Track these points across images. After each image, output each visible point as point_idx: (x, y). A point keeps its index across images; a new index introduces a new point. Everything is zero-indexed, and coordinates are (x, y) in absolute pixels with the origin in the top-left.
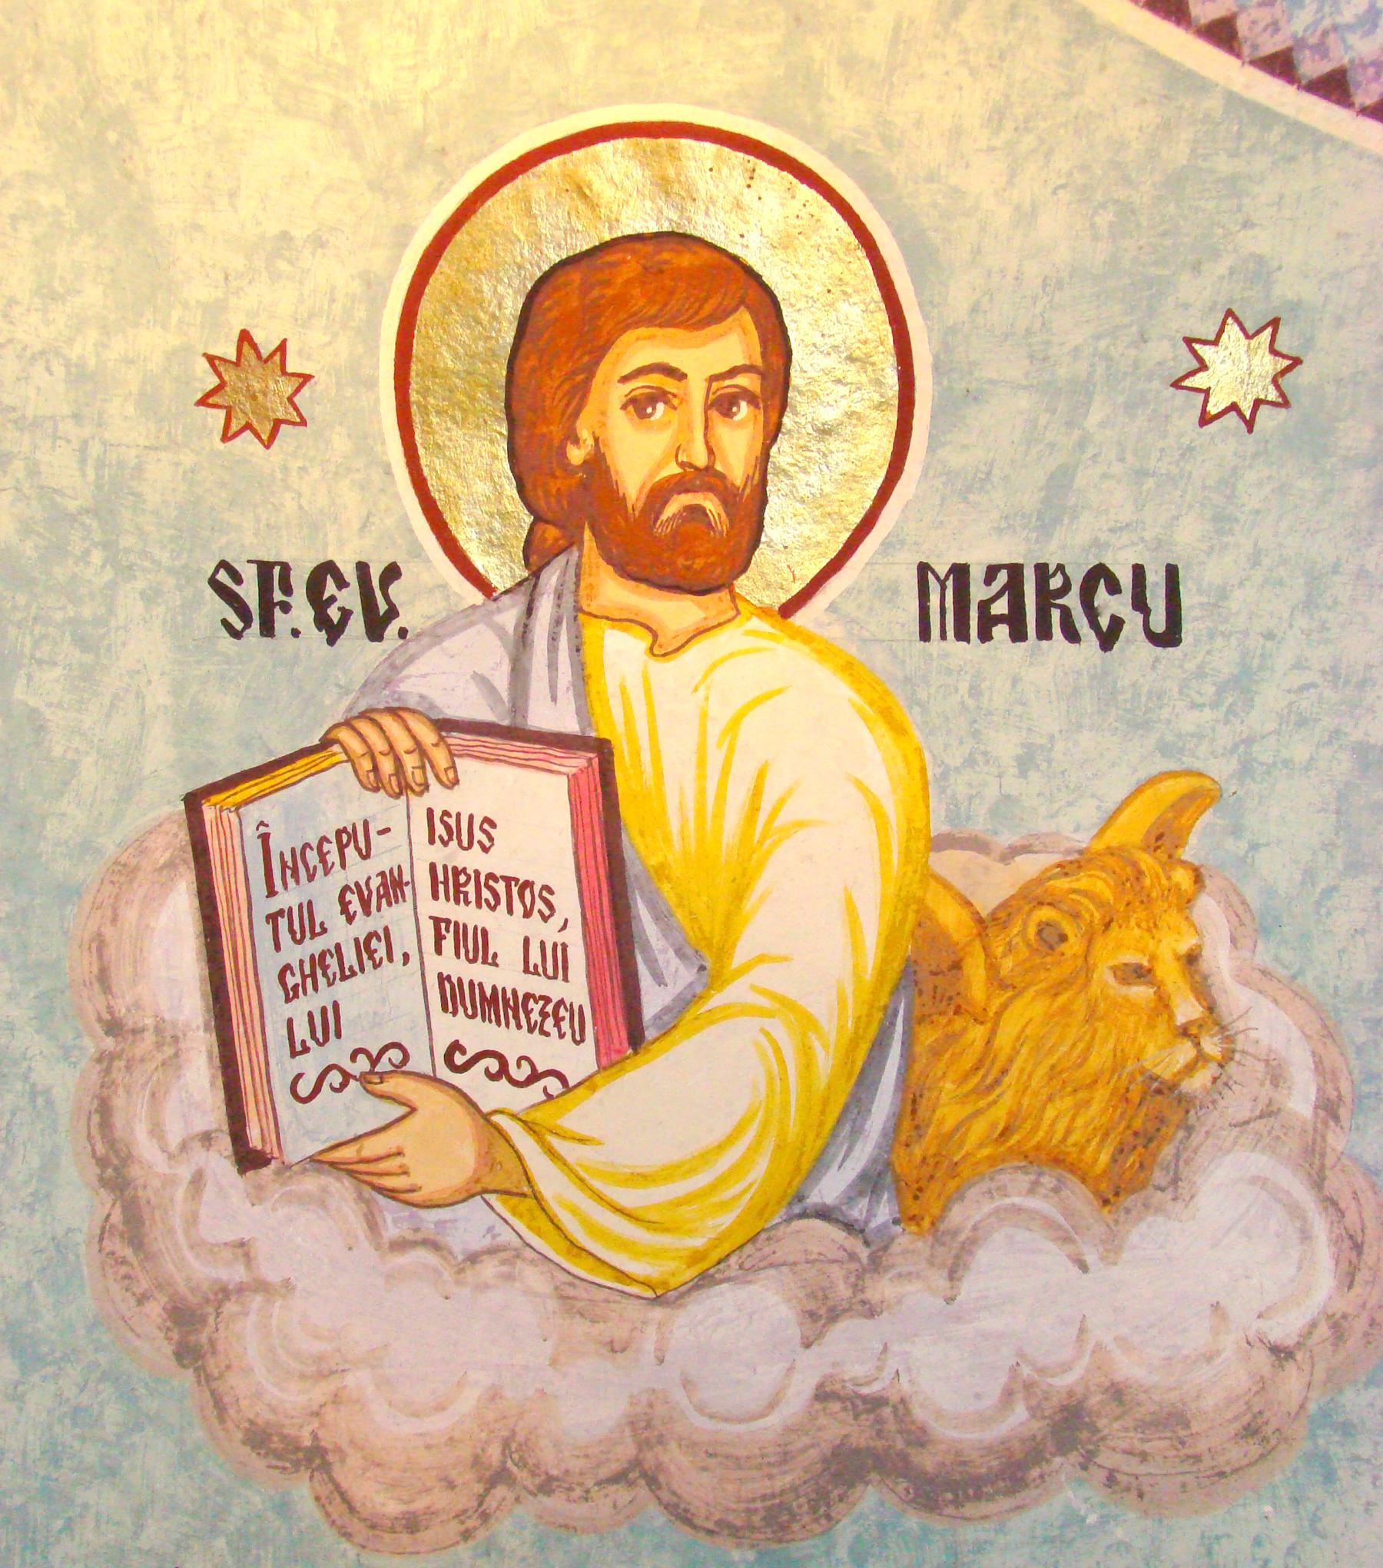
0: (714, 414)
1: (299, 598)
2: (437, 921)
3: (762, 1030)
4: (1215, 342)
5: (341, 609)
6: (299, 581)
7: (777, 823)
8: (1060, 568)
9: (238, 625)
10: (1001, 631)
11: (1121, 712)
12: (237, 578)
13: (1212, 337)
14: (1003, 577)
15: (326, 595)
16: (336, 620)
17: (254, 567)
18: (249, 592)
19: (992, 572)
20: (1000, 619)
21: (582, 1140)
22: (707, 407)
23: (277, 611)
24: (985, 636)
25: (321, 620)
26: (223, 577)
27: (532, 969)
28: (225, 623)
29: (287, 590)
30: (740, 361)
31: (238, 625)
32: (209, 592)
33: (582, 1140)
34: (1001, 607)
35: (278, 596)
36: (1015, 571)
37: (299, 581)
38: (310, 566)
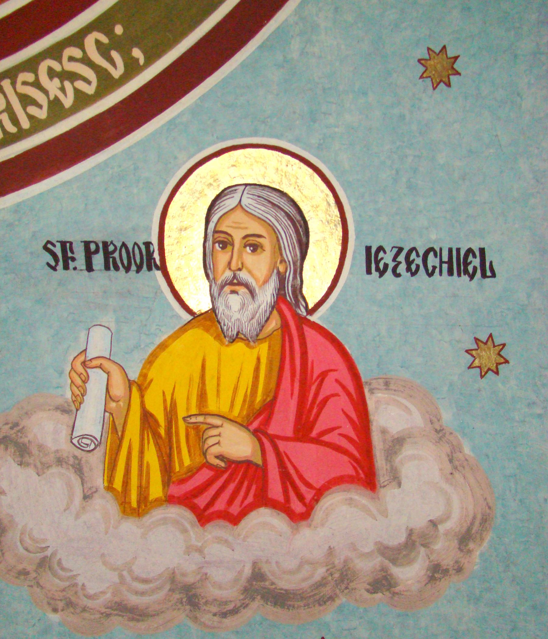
3: (340, 434)
5: (385, 263)
8: (112, 243)
9: (53, 263)
12: (54, 246)
15: (469, 261)
17: (83, 244)
18: (58, 250)
20: (445, 262)
21: (148, 448)
31: (53, 263)
33: (148, 448)
35: (70, 255)
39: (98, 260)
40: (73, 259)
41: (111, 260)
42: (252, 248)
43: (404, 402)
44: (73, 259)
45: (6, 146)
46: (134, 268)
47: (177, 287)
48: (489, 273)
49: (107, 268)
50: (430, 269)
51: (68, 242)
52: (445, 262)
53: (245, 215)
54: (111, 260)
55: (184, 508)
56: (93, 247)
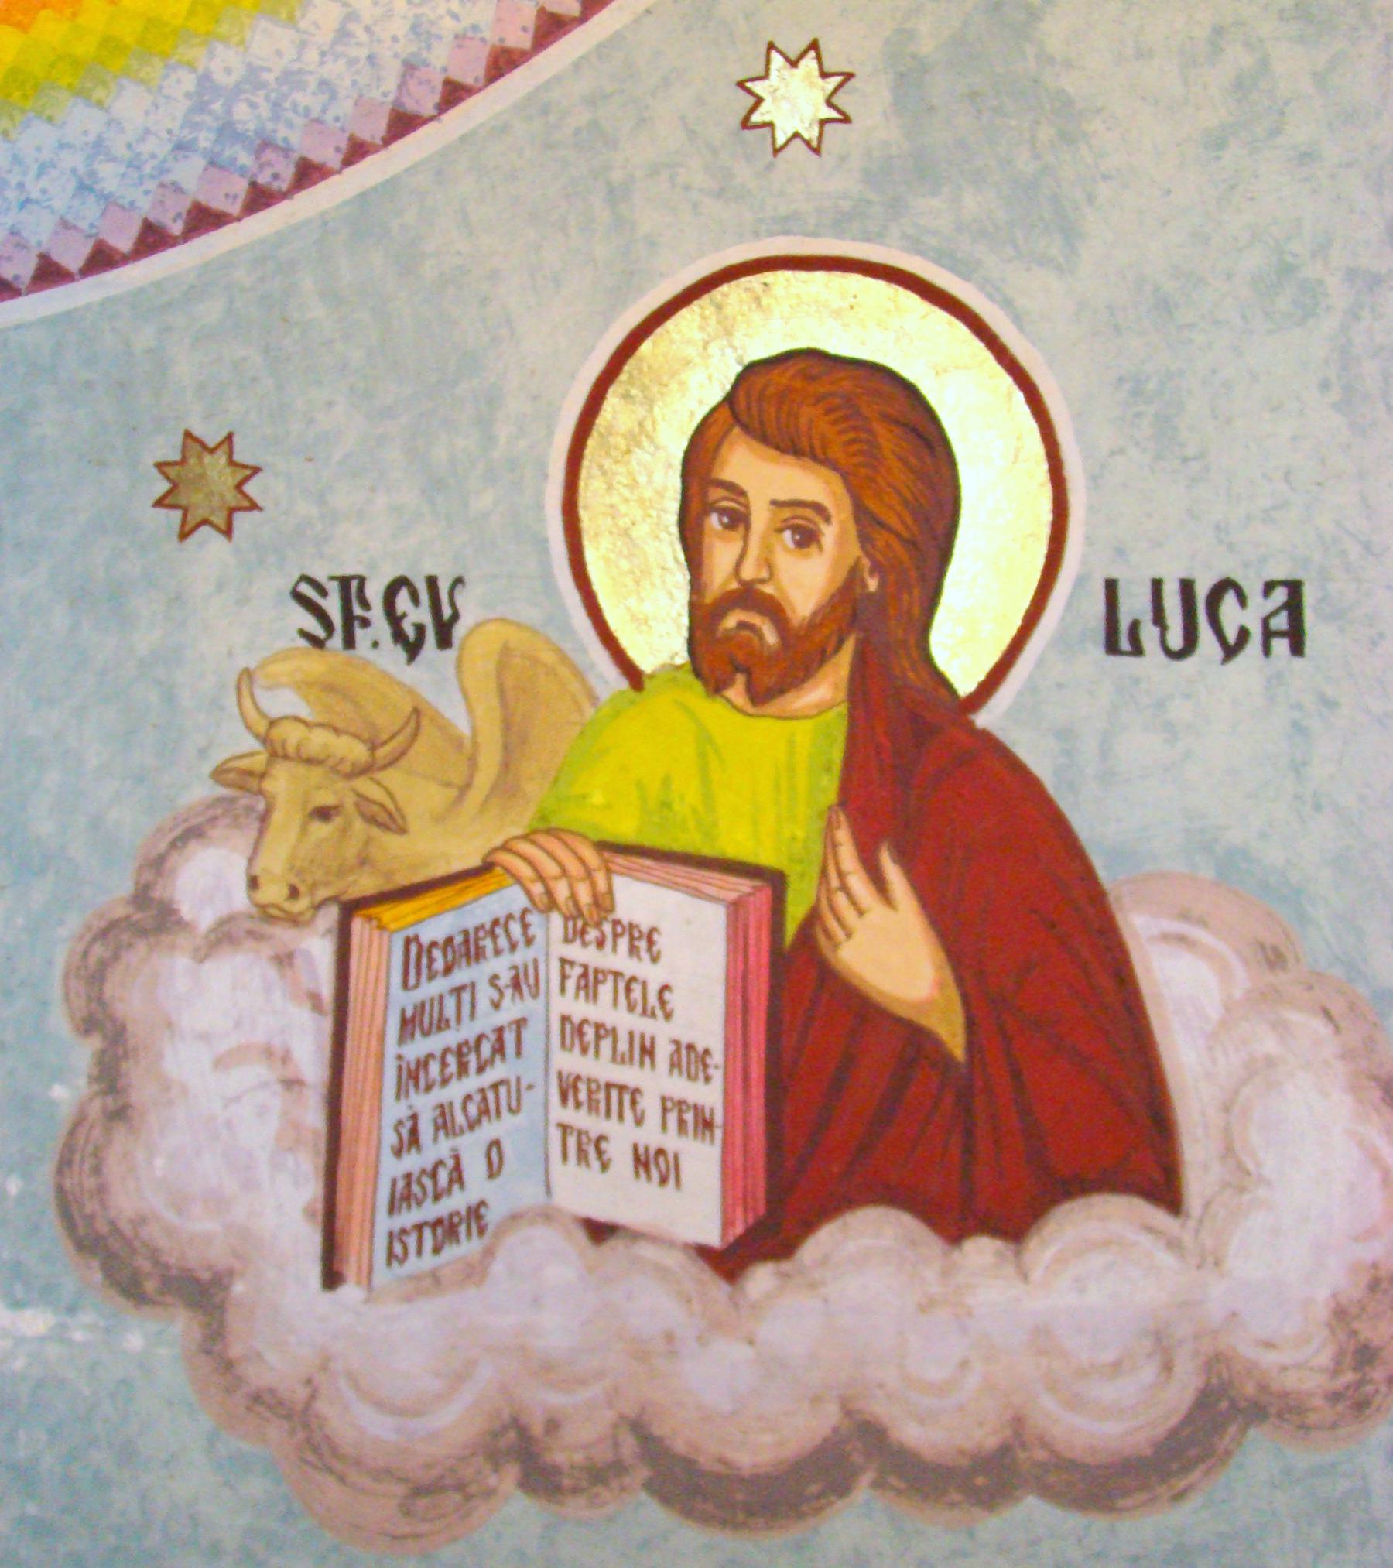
1: (377, 613)
2: (564, 962)
6: (375, 592)
9: (319, 632)
10: (1281, 646)
11: (662, 1033)
12: (323, 592)
14: (1280, 595)
18: (332, 605)
19: (1269, 588)
20: (1280, 634)
23: (356, 623)
25: (399, 636)
26: (306, 589)
27: (649, 1012)
28: (305, 634)
29: (365, 605)
31: (319, 632)
34: (1281, 622)
35: (358, 610)
37: (375, 592)
38: (386, 581)
40: (365, 623)
42: (726, 520)
44: (365, 623)
45: (256, 212)
47: (1017, 623)
48: (1125, 644)
50: (1231, 636)
51: (353, 577)
52: (1280, 634)
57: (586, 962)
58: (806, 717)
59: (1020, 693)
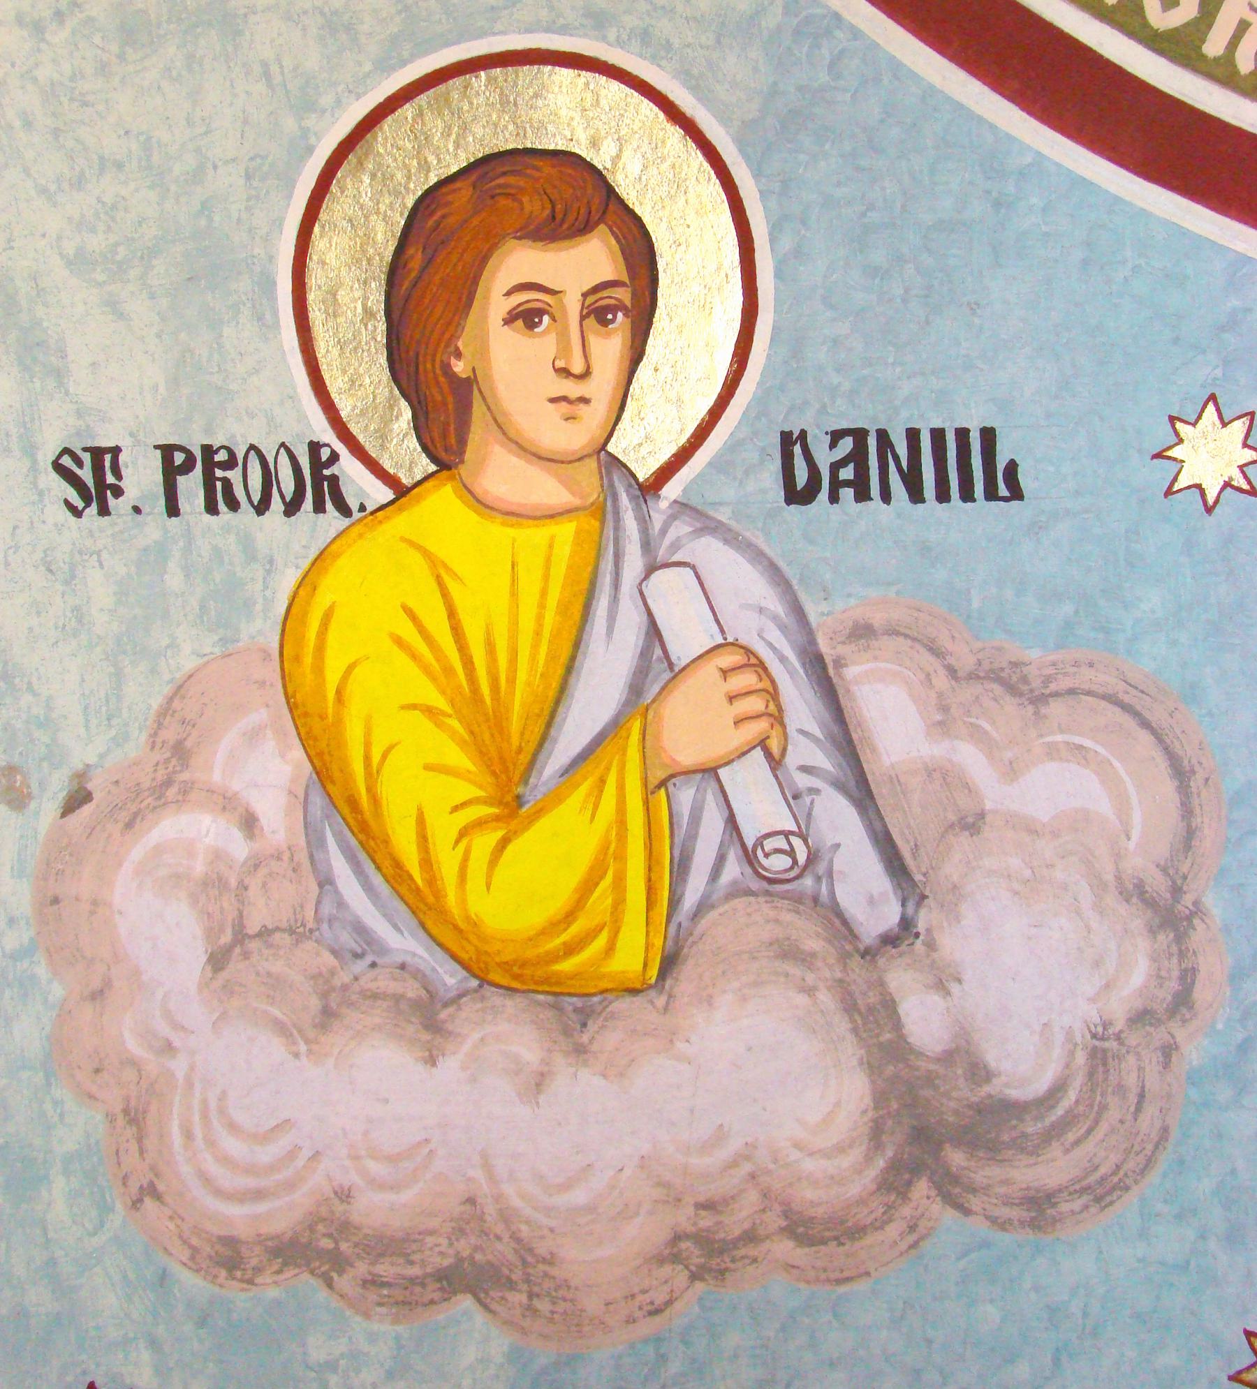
0: (591, 322)
4: (1194, 425)
7: (657, 643)
9: (80, 504)
10: (847, 494)
12: (80, 463)
13: (1192, 421)
14: (847, 445)
16: (851, 466)
17: (158, 452)
18: (86, 474)
20: (847, 483)
22: (583, 318)
24: (834, 498)
26: (66, 461)
28: (67, 503)
30: (609, 276)
31: (80, 504)
32: (54, 476)
34: (847, 473)
35: (110, 479)
36: (860, 435)
39: (191, 486)
41: (219, 485)
43: (308, 660)
46: (277, 504)
48: (1003, 491)
49: (212, 508)
52: (847, 483)
53: (557, 524)
54: (219, 485)
55: (640, 643)
56: (179, 458)
57: (466, 1197)
58: (316, 912)
59: (294, 388)
